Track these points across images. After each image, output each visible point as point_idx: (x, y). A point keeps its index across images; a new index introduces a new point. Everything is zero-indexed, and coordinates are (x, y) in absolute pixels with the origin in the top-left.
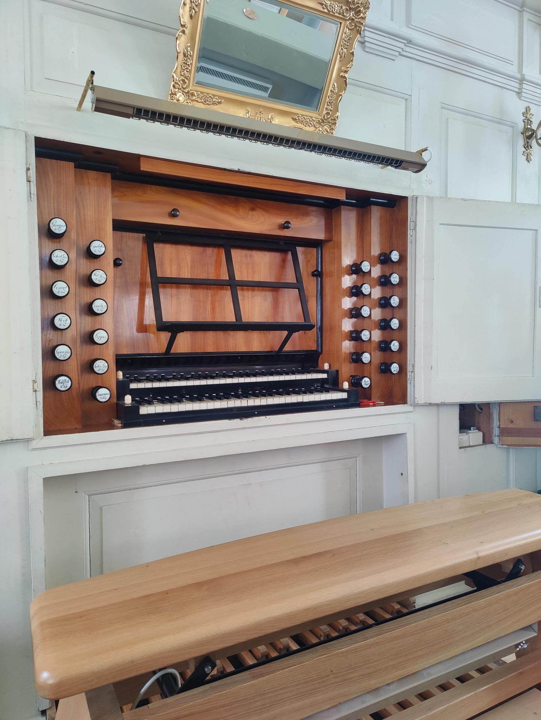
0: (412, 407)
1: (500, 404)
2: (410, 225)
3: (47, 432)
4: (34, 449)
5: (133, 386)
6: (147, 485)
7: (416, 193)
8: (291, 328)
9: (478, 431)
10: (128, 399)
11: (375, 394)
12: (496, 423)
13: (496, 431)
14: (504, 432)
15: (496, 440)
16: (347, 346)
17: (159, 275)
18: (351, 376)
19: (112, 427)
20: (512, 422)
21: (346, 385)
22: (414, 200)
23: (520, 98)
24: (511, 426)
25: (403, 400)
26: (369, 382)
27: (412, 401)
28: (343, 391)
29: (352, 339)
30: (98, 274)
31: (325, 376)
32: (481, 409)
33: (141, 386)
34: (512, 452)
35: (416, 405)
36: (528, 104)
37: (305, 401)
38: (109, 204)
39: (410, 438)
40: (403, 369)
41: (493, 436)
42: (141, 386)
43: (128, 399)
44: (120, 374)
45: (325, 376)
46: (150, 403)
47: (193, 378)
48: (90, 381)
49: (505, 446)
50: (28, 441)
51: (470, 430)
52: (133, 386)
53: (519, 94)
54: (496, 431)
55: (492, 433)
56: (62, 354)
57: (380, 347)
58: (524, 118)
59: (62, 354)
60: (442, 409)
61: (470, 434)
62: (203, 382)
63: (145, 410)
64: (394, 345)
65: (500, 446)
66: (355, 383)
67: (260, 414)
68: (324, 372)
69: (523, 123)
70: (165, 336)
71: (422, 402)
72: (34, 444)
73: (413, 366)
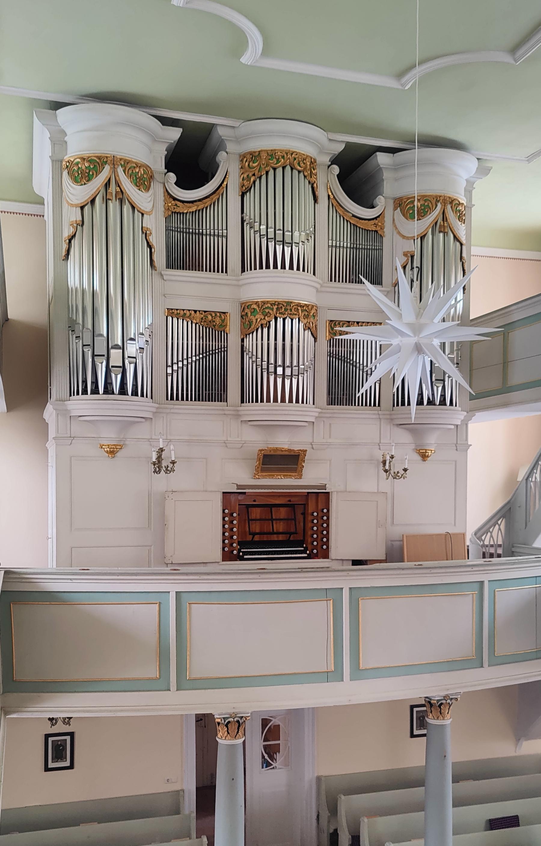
5: (242, 550)
6: (263, 498)
7: (332, 490)
8: (291, 534)
10: (241, 554)
17: (250, 518)
19: (237, 560)
33: (244, 550)
36: (383, 452)
38: (160, 213)
40: (328, 547)
42: (244, 550)
43: (241, 554)
44: (239, 547)
46: (246, 555)
47: (260, 548)
48: (232, 549)
50: (218, 562)
52: (242, 550)
53: (380, 449)
60: (344, 562)
62: (262, 550)
63: (245, 557)
67: (279, 559)
70: (251, 536)
71: (334, 558)
72: (220, 563)
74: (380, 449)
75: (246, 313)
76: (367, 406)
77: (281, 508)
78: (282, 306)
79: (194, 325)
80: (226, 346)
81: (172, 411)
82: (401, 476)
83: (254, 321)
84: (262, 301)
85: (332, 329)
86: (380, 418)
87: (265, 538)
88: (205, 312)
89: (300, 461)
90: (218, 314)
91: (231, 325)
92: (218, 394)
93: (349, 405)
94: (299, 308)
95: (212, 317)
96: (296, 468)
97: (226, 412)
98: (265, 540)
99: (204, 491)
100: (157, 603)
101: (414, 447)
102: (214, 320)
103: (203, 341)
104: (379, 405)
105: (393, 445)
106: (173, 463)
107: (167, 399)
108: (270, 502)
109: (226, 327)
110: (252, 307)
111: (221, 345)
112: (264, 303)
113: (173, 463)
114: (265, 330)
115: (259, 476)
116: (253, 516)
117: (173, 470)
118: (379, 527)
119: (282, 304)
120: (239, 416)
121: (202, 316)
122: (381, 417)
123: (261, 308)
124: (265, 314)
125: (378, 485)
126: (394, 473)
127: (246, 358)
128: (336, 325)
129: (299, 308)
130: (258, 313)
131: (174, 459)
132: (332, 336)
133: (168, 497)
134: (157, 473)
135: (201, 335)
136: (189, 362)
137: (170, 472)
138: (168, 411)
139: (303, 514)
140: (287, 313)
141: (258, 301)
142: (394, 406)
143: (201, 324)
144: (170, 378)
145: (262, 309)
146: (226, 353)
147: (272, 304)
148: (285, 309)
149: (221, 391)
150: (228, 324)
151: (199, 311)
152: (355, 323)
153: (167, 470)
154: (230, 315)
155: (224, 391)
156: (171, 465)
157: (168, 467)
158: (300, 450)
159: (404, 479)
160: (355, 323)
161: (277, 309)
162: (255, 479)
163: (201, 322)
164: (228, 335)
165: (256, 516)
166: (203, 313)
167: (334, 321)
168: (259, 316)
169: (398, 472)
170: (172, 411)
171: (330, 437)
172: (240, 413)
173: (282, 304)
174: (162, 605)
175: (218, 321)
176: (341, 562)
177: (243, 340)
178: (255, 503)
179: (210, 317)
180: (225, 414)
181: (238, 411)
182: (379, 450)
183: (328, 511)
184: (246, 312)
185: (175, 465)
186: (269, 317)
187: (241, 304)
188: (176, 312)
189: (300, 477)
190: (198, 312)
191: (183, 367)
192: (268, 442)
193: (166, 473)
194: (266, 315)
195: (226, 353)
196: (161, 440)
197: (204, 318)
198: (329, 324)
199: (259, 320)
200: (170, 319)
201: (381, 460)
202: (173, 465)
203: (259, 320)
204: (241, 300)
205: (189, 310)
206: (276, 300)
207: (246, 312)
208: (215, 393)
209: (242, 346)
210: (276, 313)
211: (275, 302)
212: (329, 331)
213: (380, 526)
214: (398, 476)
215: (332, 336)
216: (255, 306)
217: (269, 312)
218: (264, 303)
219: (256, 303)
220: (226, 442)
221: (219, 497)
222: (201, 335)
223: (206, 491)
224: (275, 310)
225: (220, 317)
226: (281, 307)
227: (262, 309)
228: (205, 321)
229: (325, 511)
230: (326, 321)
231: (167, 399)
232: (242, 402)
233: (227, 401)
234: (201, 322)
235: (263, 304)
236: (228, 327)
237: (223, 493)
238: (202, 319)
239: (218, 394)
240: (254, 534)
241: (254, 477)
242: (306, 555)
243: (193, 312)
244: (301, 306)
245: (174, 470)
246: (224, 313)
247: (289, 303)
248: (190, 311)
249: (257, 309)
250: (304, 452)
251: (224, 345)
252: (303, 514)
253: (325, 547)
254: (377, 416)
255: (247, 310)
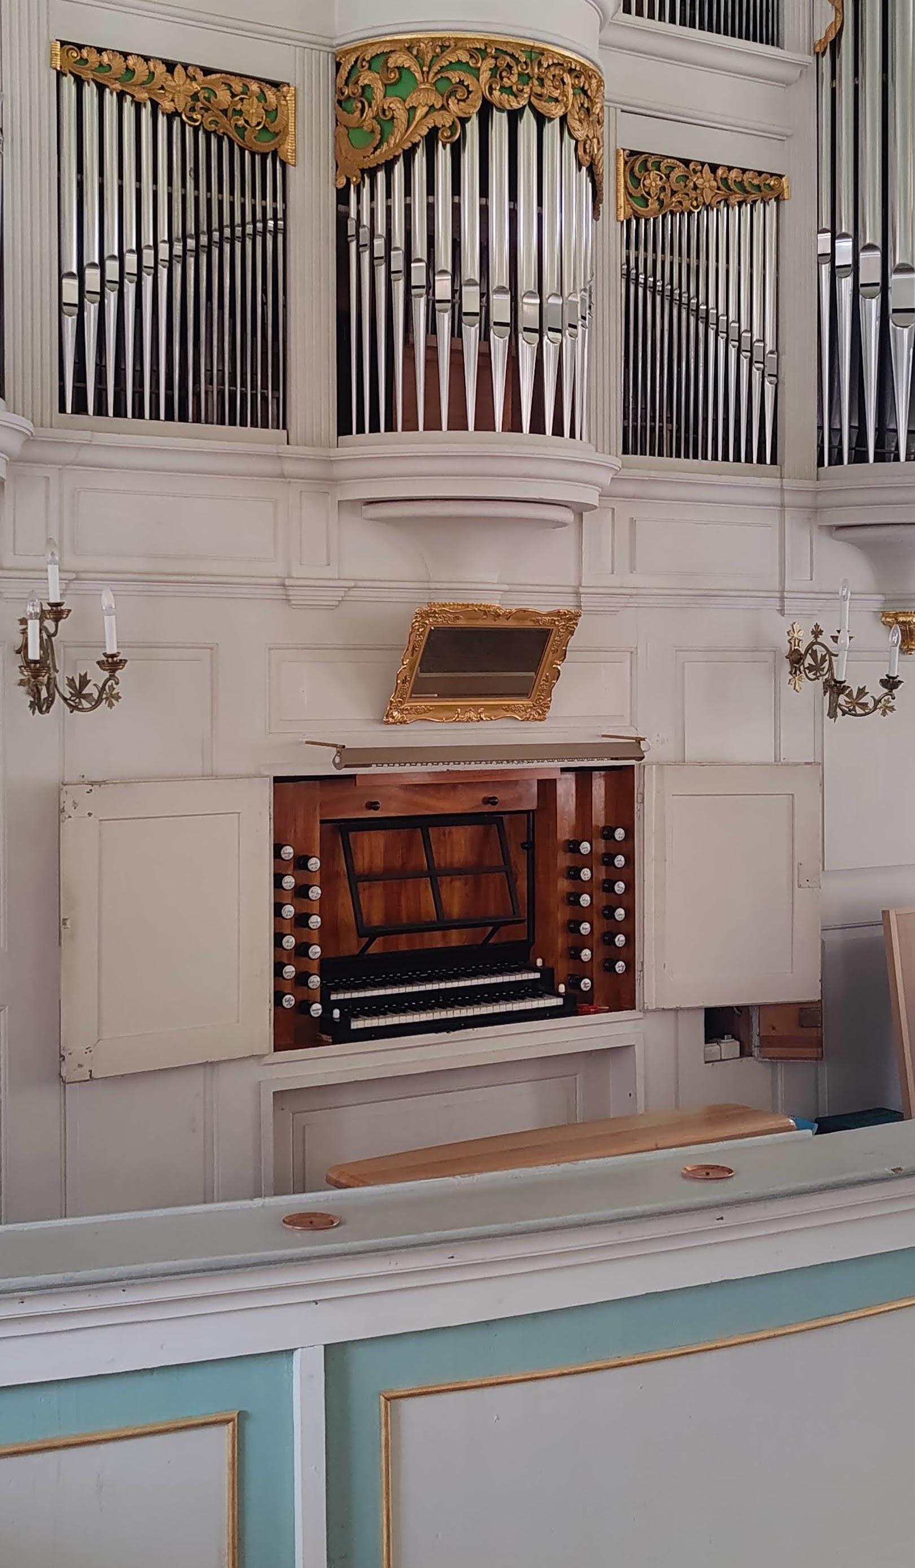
0: (642, 1013)
1: (760, 1006)
2: (637, 797)
3: (277, 1048)
4: (265, 1065)
9: (733, 1040)
10: (336, 1013)
11: (597, 996)
12: (755, 1030)
13: (756, 1040)
14: (766, 1041)
15: (756, 1051)
16: (564, 885)
18: (569, 975)
20: (774, 1028)
21: (562, 988)
22: (642, 768)
23: (783, 615)
24: (773, 1033)
25: (630, 1005)
26: (590, 984)
27: (642, 1006)
28: (558, 995)
29: (569, 877)
30: (314, 891)
31: (537, 975)
32: (741, 1012)
34: (780, 1067)
35: (645, 1011)
37: (514, 1009)
39: (638, 1050)
41: (753, 1046)
45: (537, 975)
49: (767, 1060)
51: (724, 1039)
53: (782, 612)
54: (756, 1040)
55: (752, 1043)
56: (289, 974)
57: (604, 941)
58: (790, 638)
59: (289, 974)
61: (722, 1045)
63: (356, 1024)
64: (618, 940)
65: (760, 1059)
66: (573, 984)
68: (535, 969)
69: (789, 644)
72: (268, 1060)
73: (642, 963)
74: (782, 612)
75: (363, 88)
76: (728, 460)
77: (454, 829)
78: (513, 63)
79: (162, 121)
80: (280, 215)
81: (86, 455)
82: (871, 706)
83: (401, 115)
84: (433, 39)
85: (637, 181)
86: (782, 506)
87: (403, 944)
88: (207, 71)
89: (549, 656)
90: (254, 87)
91: (299, 137)
92: (254, 397)
93: (687, 456)
94: (567, 79)
95: (233, 95)
96: (532, 682)
97: (289, 468)
98: (418, 948)
99: (204, 777)
100: (227, 1422)
101: (876, 606)
102: (238, 107)
103: (197, 187)
104: (774, 462)
105: (845, 598)
106: (112, 664)
107: (62, 409)
108: (428, 808)
109: (283, 141)
110: (391, 64)
111: (264, 209)
112: (443, 48)
113: (112, 664)
114: (443, 157)
115: (402, 711)
116: (362, 863)
117: (107, 695)
118: (800, 886)
119: (512, 56)
120: (334, 481)
121: (196, 87)
122: (788, 498)
123: (430, 68)
124: (443, 86)
125: (777, 736)
126: (71, 682)
127: (360, 263)
128: (647, 170)
129: (567, 79)
130: (416, 88)
131: (114, 651)
132: (636, 207)
133: (75, 805)
134: (41, 711)
135: (190, 165)
136: (161, 257)
137: (98, 702)
138: (68, 454)
139: (529, 847)
140: (527, 89)
141: (419, 40)
142: (820, 463)
143: (191, 118)
144: (70, 323)
145: (436, 68)
146: (280, 237)
147: (479, 52)
148: (520, 74)
149: (264, 386)
150: (291, 129)
151: (185, 66)
152: (706, 167)
153: (79, 694)
154: (295, 95)
155: (276, 388)
156: (98, 677)
157: (84, 681)
158: (558, 613)
159: (884, 714)
160: (706, 167)
161: (495, 70)
162: (387, 723)
163: (193, 109)
164: (291, 170)
165: (371, 861)
166: (199, 75)
167: (644, 153)
168: (423, 98)
169: (862, 692)
170: (86, 455)
171: (632, 569)
172: (339, 470)
173: (512, 56)
174: (252, 1429)
175: (253, 110)
176: (673, 1013)
177: (342, 196)
178: (372, 814)
179: (223, 97)
180: (282, 475)
181: (331, 462)
182: (779, 616)
183: (630, 834)
184: (364, 81)
185: (118, 674)
186: (464, 101)
187: (335, 55)
188: (94, 58)
189: (541, 711)
190: (179, 69)
191: (81, 306)
192: (432, 585)
193: (74, 708)
194: (453, 93)
195: (280, 237)
196: (53, 571)
197: (201, 95)
198: (626, 163)
199: (420, 112)
200: (69, 84)
201: (786, 649)
202: (112, 677)
203: (420, 112)
204: (335, 42)
205: (147, 59)
206: (493, 37)
207: (364, 81)
208: (244, 396)
209: (342, 220)
210: (491, 89)
211: (488, 43)
212: (626, 187)
213: (803, 883)
214: (864, 705)
215: (636, 207)
216: (401, 59)
217: (461, 82)
218: (444, 46)
219: (409, 47)
220: (288, 582)
221: (266, 793)
222: (190, 165)
223: (214, 776)
224: (485, 76)
225: (262, 97)
226: (509, 67)
227: (436, 68)
228: (207, 110)
229: (620, 834)
230: (617, 152)
231: (62, 409)
232: (344, 429)
233: (284, 428)
234: (193, 109)
235: (438, 50)
236: (290, 139)
237: (277, 780)
238: (195, 97)
239: (254, 397)
240: (368, 933)
241: (386, 718)
242: (558, 1002)
243: (161, 68)
244: (571, 71)
245: (117, 697)
246: (276, 85)
247: (536, 54)
248: (151, 64)
249: (415, 68)
250: (570, 619)
251: (275, 210)
252: (529, 847)
253: (620, 967)
254: (774, 498)
255: (366, 78)
